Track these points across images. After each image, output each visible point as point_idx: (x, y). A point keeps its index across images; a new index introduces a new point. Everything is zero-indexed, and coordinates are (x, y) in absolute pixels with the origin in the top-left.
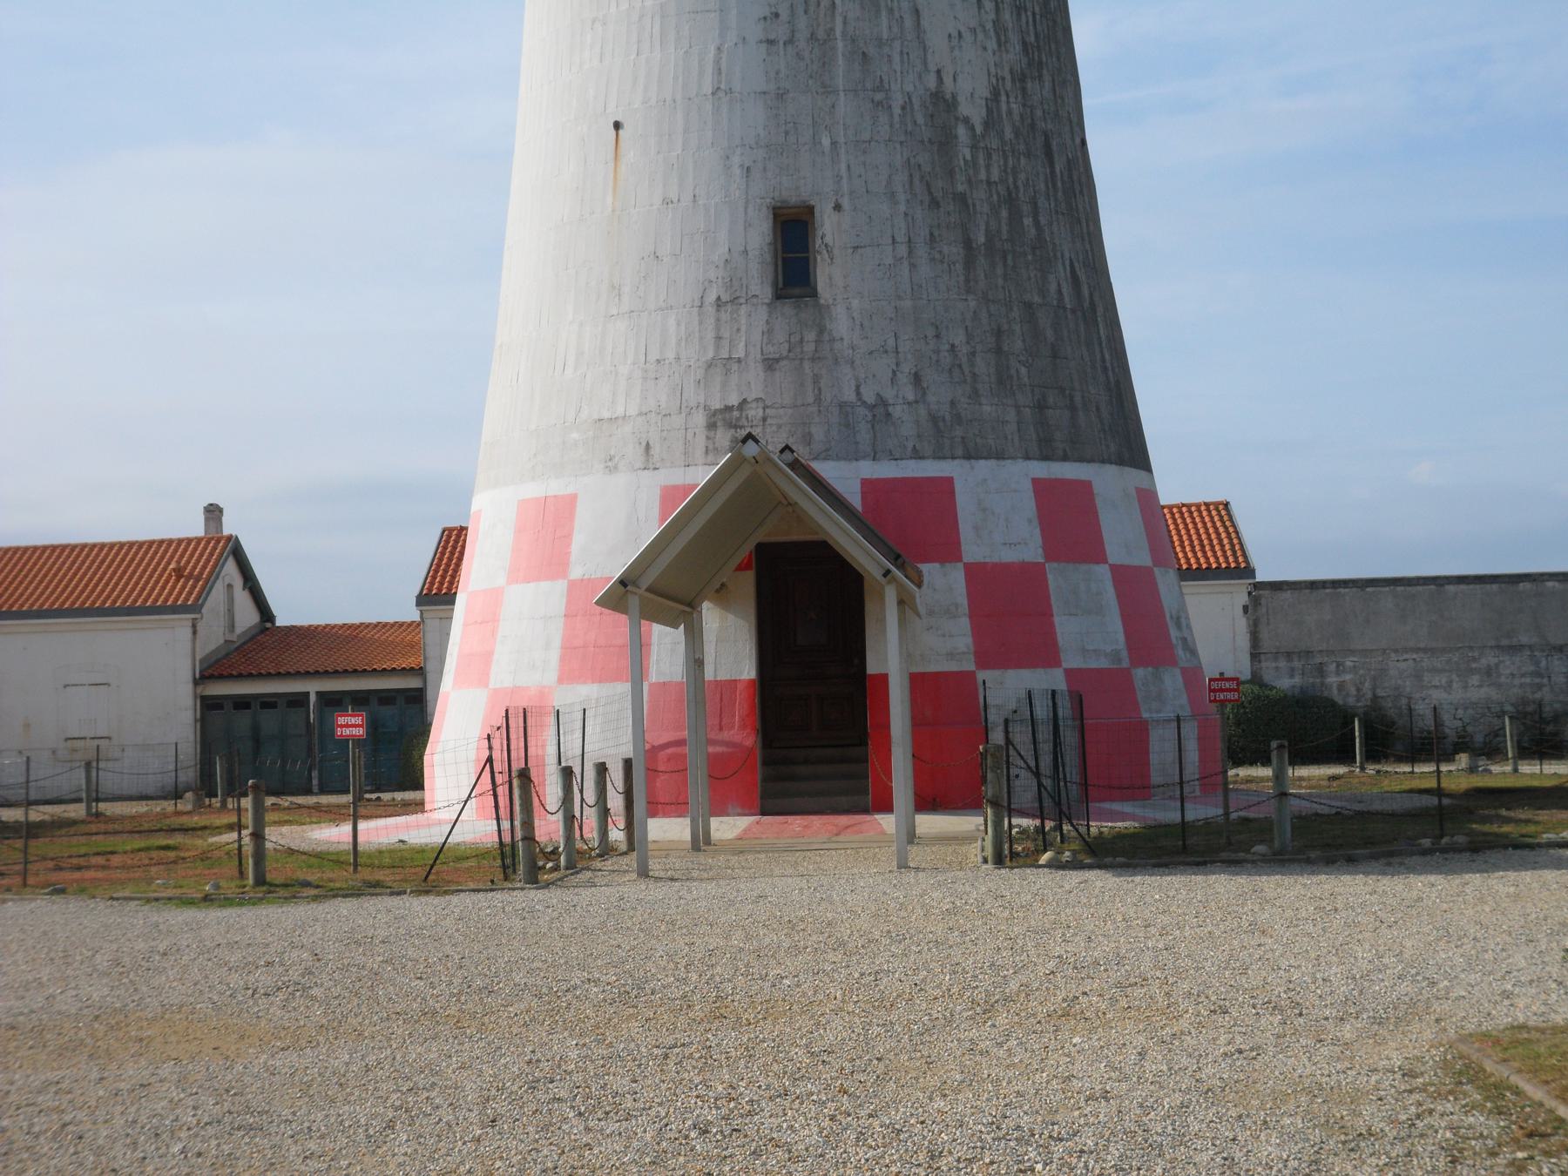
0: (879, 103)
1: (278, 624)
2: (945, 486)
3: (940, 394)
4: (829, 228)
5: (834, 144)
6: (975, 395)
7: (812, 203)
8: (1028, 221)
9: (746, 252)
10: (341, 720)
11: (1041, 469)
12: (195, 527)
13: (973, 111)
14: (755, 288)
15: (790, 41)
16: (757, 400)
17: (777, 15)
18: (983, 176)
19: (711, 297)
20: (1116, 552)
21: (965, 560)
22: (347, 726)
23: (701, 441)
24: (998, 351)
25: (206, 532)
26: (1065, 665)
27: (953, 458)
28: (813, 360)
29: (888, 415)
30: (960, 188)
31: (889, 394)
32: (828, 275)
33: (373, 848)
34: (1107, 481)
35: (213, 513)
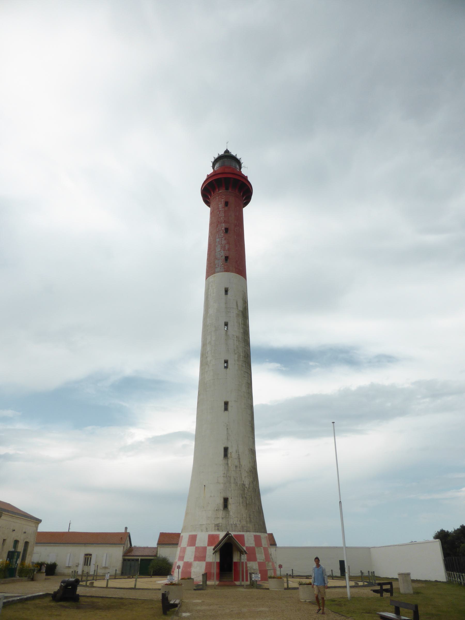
0: (236, 485)
2: (243, 536)
3: (244, 523)
4: (230, 501)
5: (231, 490)
6: (247, 523)
8: (253, 500)
9: (220, 503)
11: (255, 534)
12: (123, 531)
13: (247, 486)
14: (221, 508)
15: (226, 477)
17: (225, 473)
18: (248, 494)
20: (263, 546)
23: (214, 528)
24: (250, 517)
25: (125, 531)
26: (258, 561)
27: (244, 532)
28: (228, 518)
29: (237, 526)
30: (246, 496)
31: (237, 523)
32: (230, 507)
33: (208, 584)
34: (262, 535)
35: (126, 528)
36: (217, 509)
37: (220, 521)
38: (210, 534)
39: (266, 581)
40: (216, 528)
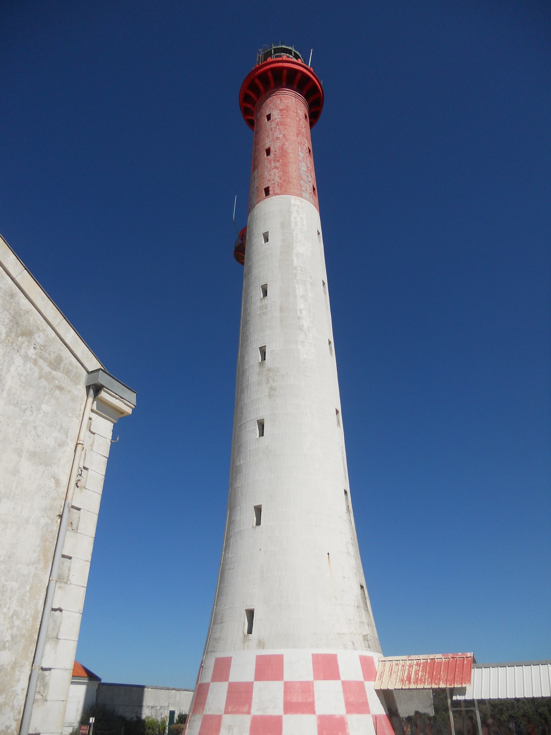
1: (102, 681)
21: (343, 678)
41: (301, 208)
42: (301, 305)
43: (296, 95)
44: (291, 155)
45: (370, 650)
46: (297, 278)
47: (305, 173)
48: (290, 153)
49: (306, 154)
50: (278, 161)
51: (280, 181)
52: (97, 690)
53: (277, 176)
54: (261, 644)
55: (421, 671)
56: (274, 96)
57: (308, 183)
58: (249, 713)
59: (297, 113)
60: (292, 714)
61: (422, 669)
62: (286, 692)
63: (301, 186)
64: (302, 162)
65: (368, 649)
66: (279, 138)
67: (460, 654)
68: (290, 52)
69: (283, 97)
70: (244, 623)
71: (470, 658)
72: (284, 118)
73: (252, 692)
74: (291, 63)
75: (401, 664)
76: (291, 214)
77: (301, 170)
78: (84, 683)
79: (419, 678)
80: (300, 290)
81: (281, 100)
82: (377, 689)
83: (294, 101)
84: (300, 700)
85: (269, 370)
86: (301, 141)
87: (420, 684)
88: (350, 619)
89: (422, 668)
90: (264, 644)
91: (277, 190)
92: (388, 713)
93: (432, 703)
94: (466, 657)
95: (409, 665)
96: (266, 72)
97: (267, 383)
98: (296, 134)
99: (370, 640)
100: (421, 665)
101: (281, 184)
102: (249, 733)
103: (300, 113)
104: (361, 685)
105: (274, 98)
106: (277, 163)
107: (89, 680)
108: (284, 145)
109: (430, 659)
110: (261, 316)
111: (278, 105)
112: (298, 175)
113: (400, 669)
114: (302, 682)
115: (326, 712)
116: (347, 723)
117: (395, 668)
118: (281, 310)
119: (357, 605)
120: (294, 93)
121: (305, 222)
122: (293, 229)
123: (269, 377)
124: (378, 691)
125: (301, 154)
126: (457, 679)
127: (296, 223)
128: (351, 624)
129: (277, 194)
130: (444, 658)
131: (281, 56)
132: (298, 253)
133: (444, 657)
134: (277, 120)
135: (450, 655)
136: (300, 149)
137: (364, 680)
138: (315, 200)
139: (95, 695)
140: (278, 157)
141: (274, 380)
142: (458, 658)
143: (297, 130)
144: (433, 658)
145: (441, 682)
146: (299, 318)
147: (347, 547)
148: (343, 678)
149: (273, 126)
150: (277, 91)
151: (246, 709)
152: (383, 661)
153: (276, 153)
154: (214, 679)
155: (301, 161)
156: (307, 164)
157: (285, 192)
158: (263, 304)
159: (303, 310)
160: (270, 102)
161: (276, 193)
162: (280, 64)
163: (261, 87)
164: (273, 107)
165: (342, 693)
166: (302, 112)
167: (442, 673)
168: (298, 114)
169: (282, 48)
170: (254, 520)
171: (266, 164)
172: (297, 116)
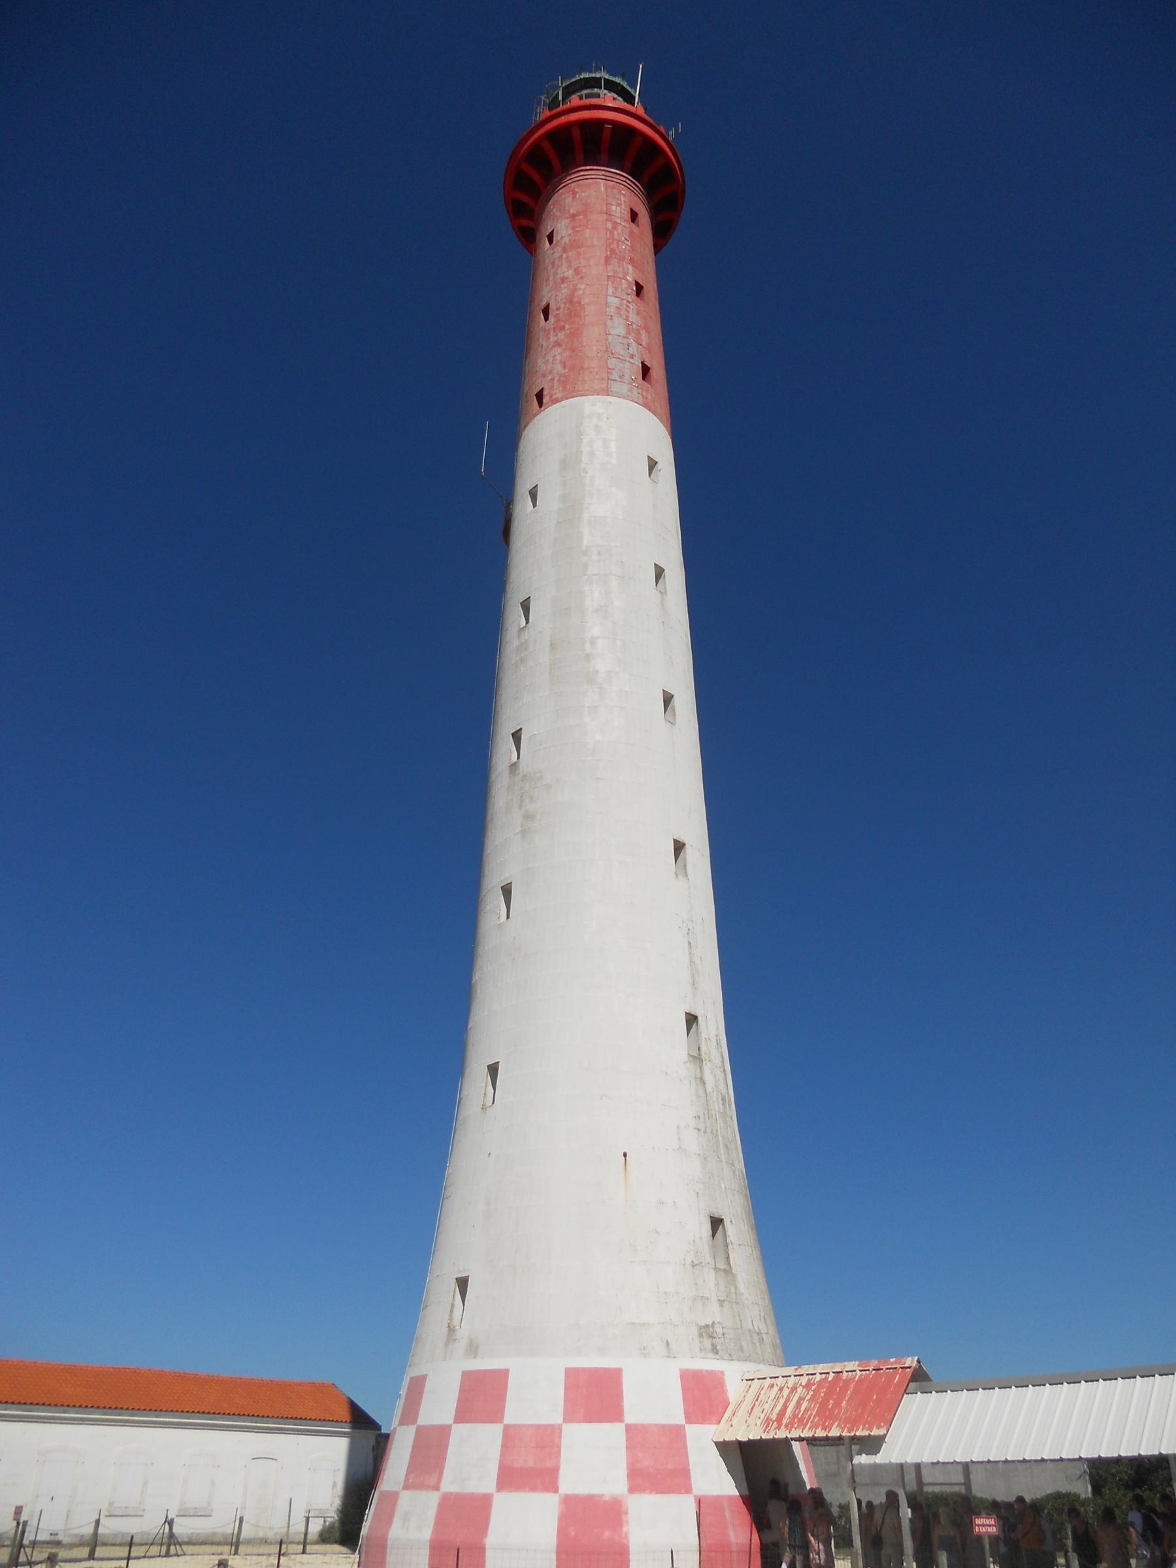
1: (382, 1431)
7: (723, 1217)
9: (701, 1238)
10: (978, 1521)
16: (719, 1323)
19: (688, 1261)
21: (630, 1417)
22: (983, 1525)
36: (695, 1262)
37: (713, 1314)
38: (687, 1370)
39: (757, 1528)
40: (707, 1343)
41: (606, 419)
42: (595, 628)
43: (607, 174)
44: (590, 310)
45: (718, 1357)
46: (589, 572)
47: (621, 340)
48: (588, 305)
49: (625, 297)
50: (563, 328)
51: (564, 372)
52: (373, 1447)
53: (558, 362)
54: (473, 1349)
55: (809, 1400)
56: (561, 191)
57: (628, 359)
58: (437, 1488)
59: (608, 213)
60: (511, 1492)
61: (812, 1395)
62: (505, 1446)
63: (609, 371)
64: (615, 319)
65: (711, 1355)
66: (567, 278)
67: (892, 1360)
68: (595, 83)
69: (579, 186)
70: (453, 1306)
71: (908, 1370)
72: (578, 231)
73: (447, 1446)
74: (586, 110)
75: (779, 1386)
76: (582, 437)
77: (610, 336)
78: (345, 1433)
79: (800, 1416)
80: (593, 596)
81: (574, 194)
82: (719, 1440)
83: (602, 189)
84: (531, 1463)
85: (525, 778)
86: (615, 272)
87: (796, 1429)
88: (666, 1293)
89: (812, 1393)
90: (477, 1348)
91: (558, 390)
92: (746, 1492)
93: (1085, 1472)
94: (902, 1368)
95: (791, 1388)
96: (537, 144)
97: (521, 807)
98: (603, 261)
99: (721, 1335)
100: (813, 1387)
101: (565, 377)
102: (432, 1529)
103: (616, 212)
104: (676, 1433)
105: (562, 194)
106: (559, 334)
107: (354, 1428)
108: (575, 289)
109: (833, 1373)
110: (516, 667)
111: (567, 208)
112: (603, 349)
113: (772, 1397)
114: (538, 1427)
115: (582, 1489)
116: (626, 1513)
117: (765, 1394)
118: (553, 647)
119: (692, 1261)
120: (603, 170)
121: (613, 447)
122: (584, 469)
123: (523, 793)
124: (724, 1448)
125: (614, 301)
126: (868, 1417)
127: (592, 454)
128: (666, 1303)
129: (556, 401)
130: (860, 1371)
131: (598, 96)
132: (592, 519)
133: (860, 1369)
134: (563, 242)
135: (874, 1363)
136: (610, 291)
137: (686, 1423)
138: (644, 393)
139: (371, 1456)
140: (562, 321)
141: (532, 799)
142: (887, 1369)
143: (606, 248)
144: (840, 1370)
145: (836, 1424)
146: (588, 657)
147: (679, 1138)
148: (630, 1417)
149: (557, 255)
150: (566, 177)
151: (432, 1481)
152: (749, 1380)
153: (558, 312)
154: (401, 1423)
155: (611, 316)
156: (627, 319)
157: (573, 391)
158: (522, 640)
159: (598, 638)
160: (554, 205)
161: (555, 399)
162: (563, 119)
163: (536, 177)
164: (558, 214)
165: (624, 1450)
166: (624, 207)
167: (844, 1404)
168: (610, 215)
169: (581, 79)
170: (488, 1095)
171: (541, 341)
172: (607, 220)
